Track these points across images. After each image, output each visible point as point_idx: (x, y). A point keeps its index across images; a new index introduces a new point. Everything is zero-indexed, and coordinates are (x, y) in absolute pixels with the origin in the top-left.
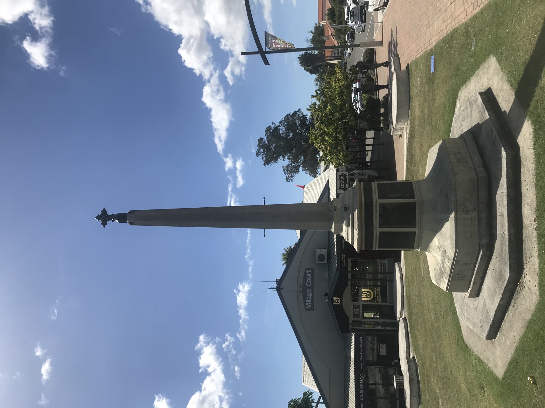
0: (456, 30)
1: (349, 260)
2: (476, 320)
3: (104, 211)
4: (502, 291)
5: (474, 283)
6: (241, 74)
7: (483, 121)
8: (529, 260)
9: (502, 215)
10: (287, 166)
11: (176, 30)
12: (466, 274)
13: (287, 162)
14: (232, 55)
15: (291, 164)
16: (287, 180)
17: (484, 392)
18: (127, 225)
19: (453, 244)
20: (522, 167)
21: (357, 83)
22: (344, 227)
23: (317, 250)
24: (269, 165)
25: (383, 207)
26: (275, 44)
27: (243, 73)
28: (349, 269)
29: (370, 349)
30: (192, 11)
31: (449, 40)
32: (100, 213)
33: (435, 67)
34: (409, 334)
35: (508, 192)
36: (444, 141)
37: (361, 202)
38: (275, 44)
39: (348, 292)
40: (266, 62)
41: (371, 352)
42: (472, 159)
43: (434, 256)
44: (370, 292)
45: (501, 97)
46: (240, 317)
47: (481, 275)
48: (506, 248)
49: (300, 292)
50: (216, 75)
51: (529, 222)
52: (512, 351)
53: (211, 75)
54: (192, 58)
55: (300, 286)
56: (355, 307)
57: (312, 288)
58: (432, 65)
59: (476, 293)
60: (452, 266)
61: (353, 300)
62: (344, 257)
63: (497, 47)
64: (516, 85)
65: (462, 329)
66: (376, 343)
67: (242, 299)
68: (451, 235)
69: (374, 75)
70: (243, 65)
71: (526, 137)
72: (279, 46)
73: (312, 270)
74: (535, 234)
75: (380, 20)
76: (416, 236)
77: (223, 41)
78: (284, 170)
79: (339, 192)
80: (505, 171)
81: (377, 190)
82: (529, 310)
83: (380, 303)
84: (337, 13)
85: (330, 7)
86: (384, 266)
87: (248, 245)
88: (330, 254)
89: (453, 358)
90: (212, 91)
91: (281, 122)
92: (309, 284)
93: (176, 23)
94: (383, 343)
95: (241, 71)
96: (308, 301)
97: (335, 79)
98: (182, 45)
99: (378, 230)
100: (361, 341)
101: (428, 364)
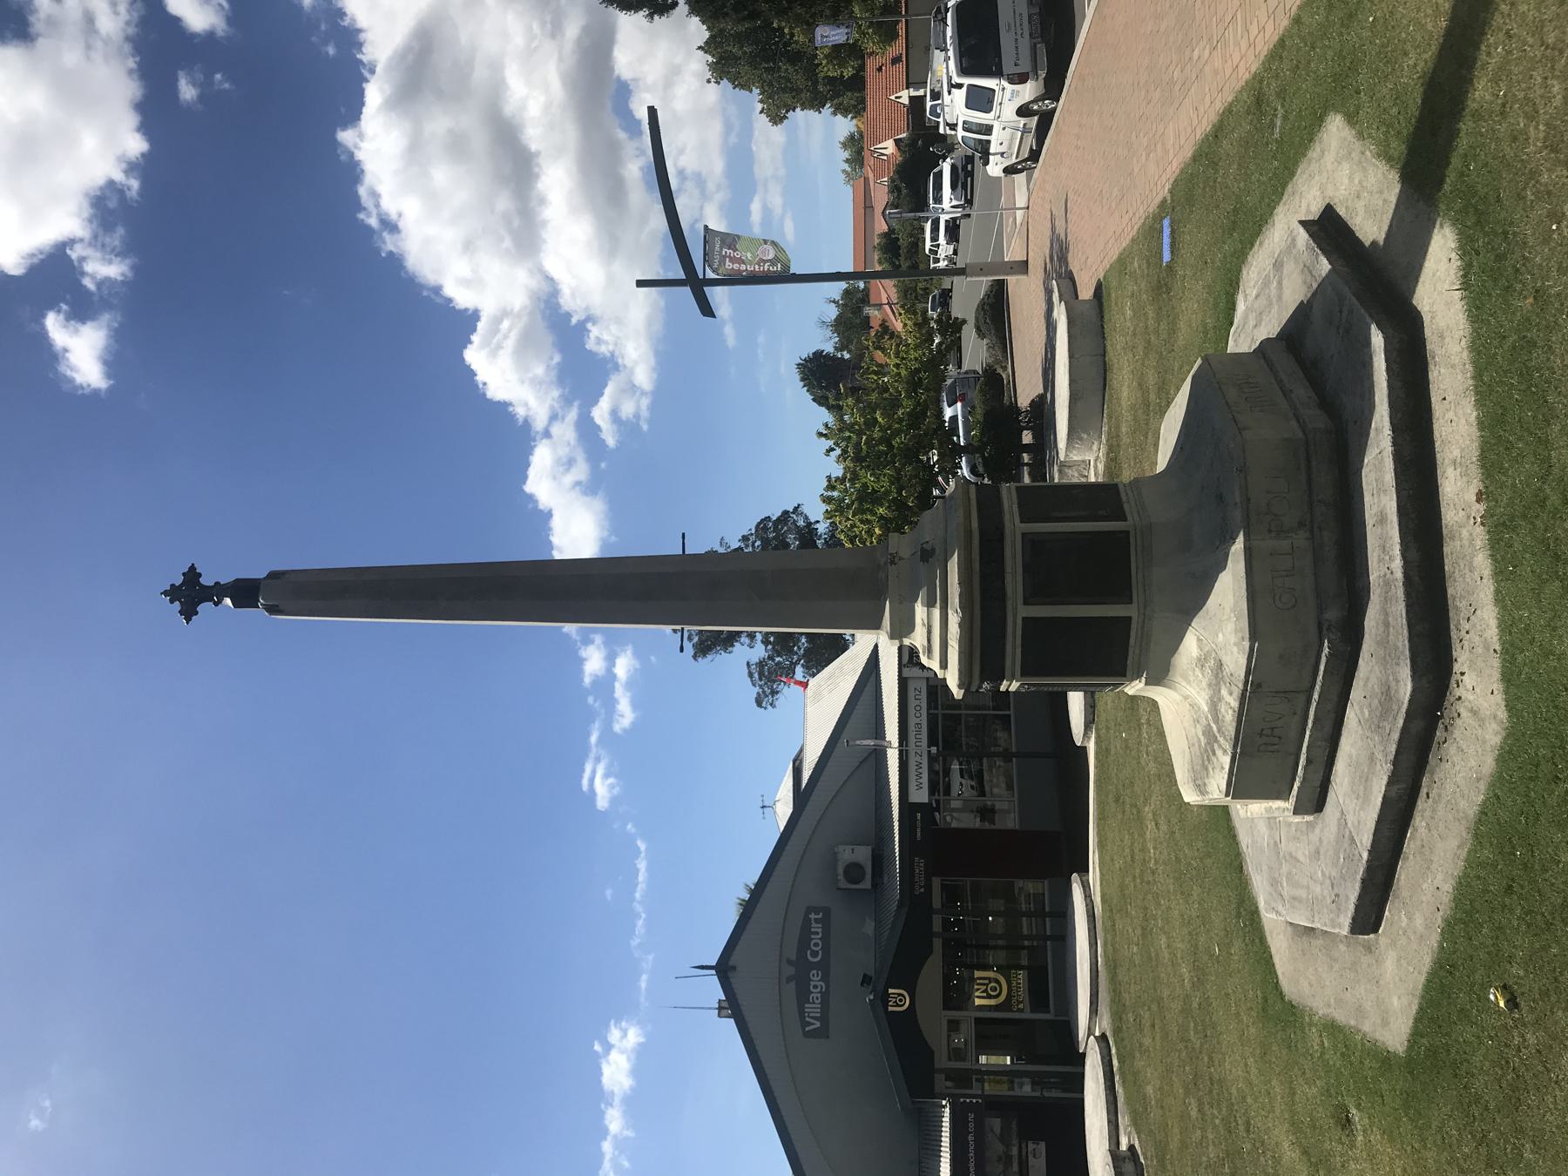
0: (1229, 111)
1: (936, 882)
2: (1318, 889)
3: (192, 575)
4: (1393, 748)
5: (1309, 761)
6: (637, 416)
7: (1315, 286)
8: (1467, 627)
9: (1382, 519)
10: (761, 664)
11: (463, 298)
12: (1280, 742)
13: (759, 652)
14: (616, 368)
15: (771, 658)
16: (759, 703)
17: (1351, 1134)
18: (258, 614)
19: (1241, 630)
20: (1431, 367)
21: (959, 404)
22: (920, 611)
23: (841, 848)
24: (709, 657)
25: (1033, 544)
26: (733, 260)
27: (645, 413)
28: (937, 903)
29: (1000, 1159)
30: (508, 243)
31: (1207, 154)
32: (179, 580)
33: (1173, 245)
34: (1117, 1078)
35: (1394, 444)
36: (1206, 360)
37: (969, 533)
38: (733, 260)
39: (932, 973)
40: (707, 310)
41: (1001, 1168)
42: (1286, 394)
43: (1186, 698)
44: (997, 981)
45: (1361, 211)
46: (604, 1132)
47: (1328, 728)
48: (1399, 608)
49: (789, 980)
50: (573, 415)
51: (1462, 513)
52: (1434, 939)
53: (554, 417)
54: (501, 371)
55: (789, 962)
56: (954, 1026)
57: (824, 966)
58: (1166, 240)
59: (1314, 801)
60: (1242, 704)
61: (947, 1006)
62: (920, 865)
63: (1340, 93)
64: (1399, 148)
65: (1277, 960)
66: (1015, 1141)
67: (616, 1072)
68: (1236, 603)
69: (1005, 368)
70: (643, 393)
71: (1439, 289)
72: (743, 267)
73: (827, 912)
74: (1480, 535)
75: (1021, 201)
76: (1133, 634)
77: (594, 331)
78: (751, 675)
79: (907, 672)
80: (1385, 384)
81: (1015, 500)
82: (1478, 779)
83: (1028, 1015)
84: (903, 242)
85: (885, 228)
86: (1039, 898)
87: (639, 908)
88: (880, 859)
89: (1254, 1071)
90: (558, 462)
91: (745, 538)
92: (815, 954)
93: (466, 283)
94: (1036, 1140)
95: (638, 407)
96: (813, 1009)
97: (898, 345)
98: (474, 338)
99: (1019, 611)
100: (971, 1126)
101: (1174, 1145)
